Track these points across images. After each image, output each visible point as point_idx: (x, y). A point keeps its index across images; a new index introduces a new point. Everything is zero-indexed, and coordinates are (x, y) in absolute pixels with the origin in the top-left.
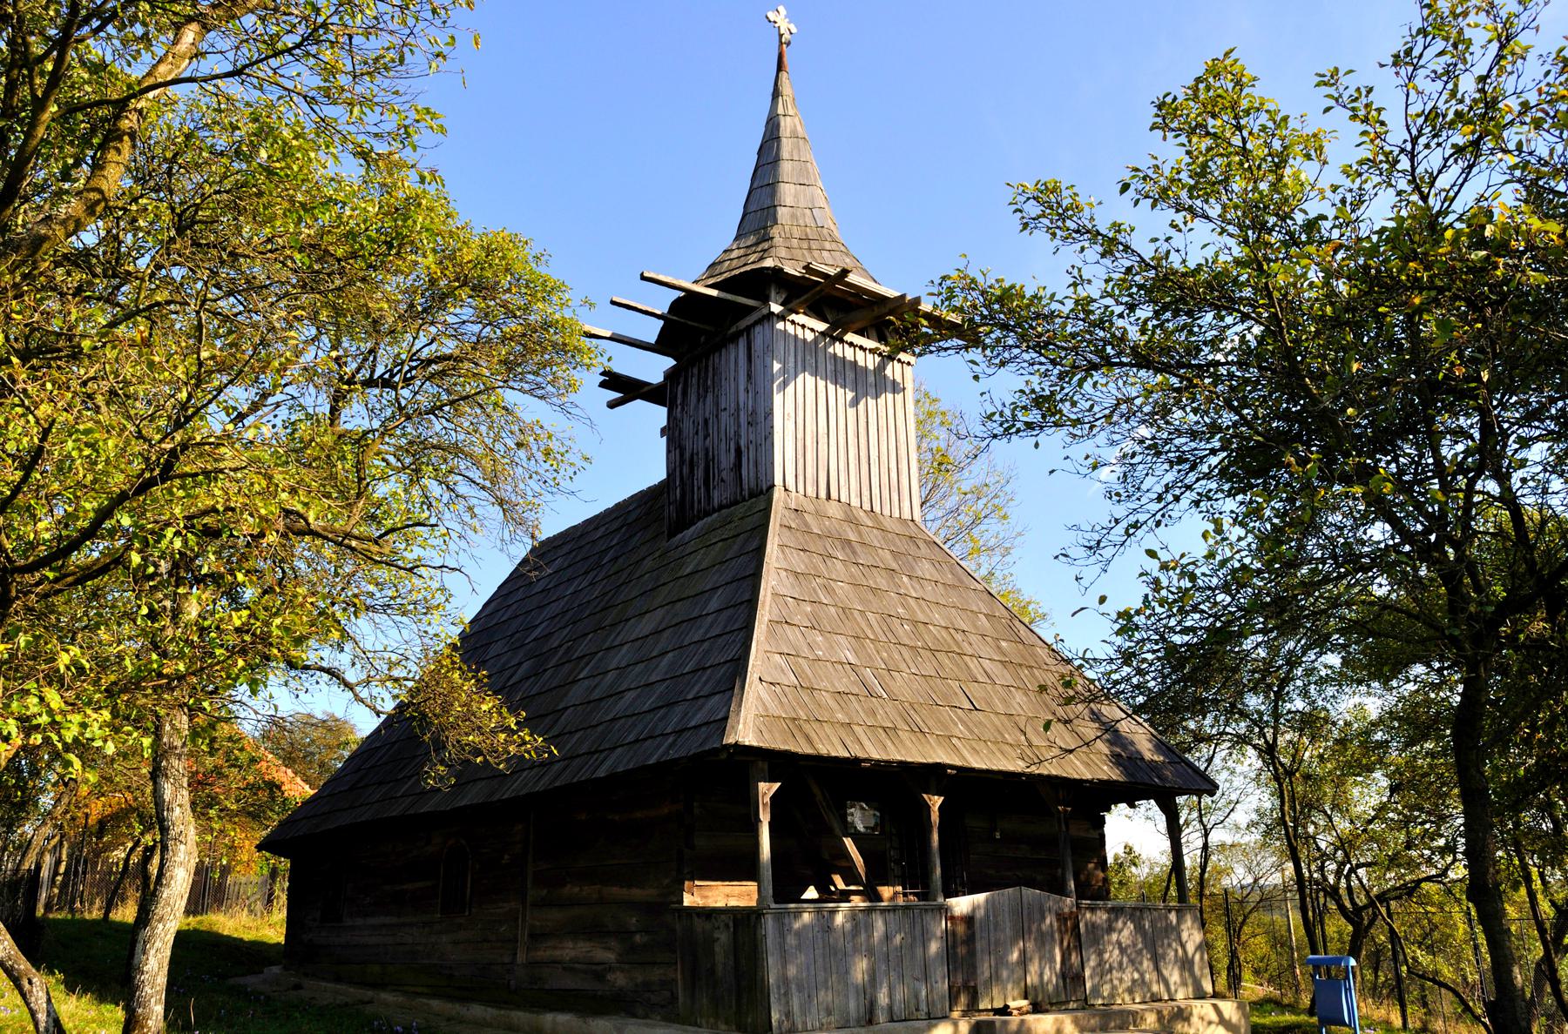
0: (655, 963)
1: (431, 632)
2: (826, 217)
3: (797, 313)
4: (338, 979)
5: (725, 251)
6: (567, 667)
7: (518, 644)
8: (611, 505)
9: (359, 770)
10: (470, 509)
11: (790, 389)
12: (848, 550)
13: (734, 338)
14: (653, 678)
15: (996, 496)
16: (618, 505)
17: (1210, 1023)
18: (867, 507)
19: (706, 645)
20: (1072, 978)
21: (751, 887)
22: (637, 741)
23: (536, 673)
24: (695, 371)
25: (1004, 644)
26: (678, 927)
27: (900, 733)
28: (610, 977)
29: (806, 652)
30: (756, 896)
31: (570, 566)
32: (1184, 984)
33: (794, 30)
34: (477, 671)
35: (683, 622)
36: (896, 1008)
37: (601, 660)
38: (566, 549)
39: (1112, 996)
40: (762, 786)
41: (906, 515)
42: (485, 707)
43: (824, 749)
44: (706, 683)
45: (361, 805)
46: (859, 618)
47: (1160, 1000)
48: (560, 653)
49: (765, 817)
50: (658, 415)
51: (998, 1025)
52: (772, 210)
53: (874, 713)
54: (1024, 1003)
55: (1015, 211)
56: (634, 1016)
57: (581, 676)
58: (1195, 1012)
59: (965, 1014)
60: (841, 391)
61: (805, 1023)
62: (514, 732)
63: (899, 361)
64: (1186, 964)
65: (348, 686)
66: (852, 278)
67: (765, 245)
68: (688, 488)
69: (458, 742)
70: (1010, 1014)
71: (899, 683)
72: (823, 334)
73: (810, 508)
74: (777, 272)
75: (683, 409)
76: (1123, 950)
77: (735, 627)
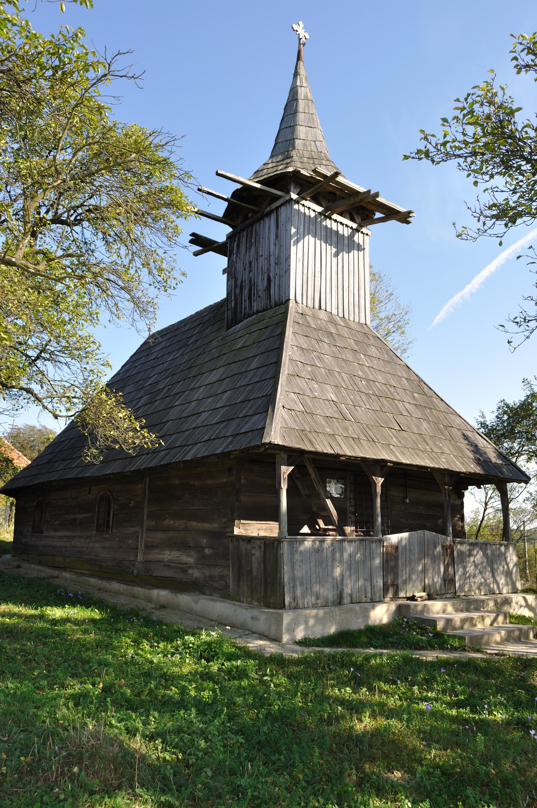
0: (216, 566)
1: (89, 369)
2: (323, 147)
3: (306, 200)
4: (40, 564)
5: (264, 164)
6: (168, 399)
7: (140, 387)
8: (193, 313)
9: (53, 453)
10: (116, 304)
11: (300, 244)
12: (331, 338)
13: (269, 214)
14: (218, 405)
15: (399, 321)
16: (197, 313)
17: (521, 606)
18: (341, 315)
19: (250, 387)
20: (449, 581)
21: (274, 525)
22: (209, 440)
23: (150, 403)
24: (245, 234)
25: (416, 395)
26: (231, 546)
27: (362, 441)
28: (190, 571)
29: (308, 393)
30: (277, 531)
31: (170, 345)
32: (507, 584)
33: (307, 37)
34: (116, 392)
35: (236, 374)
36: (354, 596)
37: (188, 395)
38: (168, 336)
39: (470, 590)
40: (284, 468)
41: (362, 321)
42: (120, 415)
43: (320, 448)
44: (250, 408)
45: (53, 472)
46: (338, 376)
47: (494, 593)
48: (164, 392)
49: (284, 486)
50: (222, 261)
51: (412, 607)
52: (292, 141)
53: (347, 430)
54: (424, 594)
55: (513, 59)
56: (204, 594)
57: (176, 404)
58: (514, 600)
59: (392, 599)
60: (329, 247)
61: (303, 603)
62: (138, 431)
63: (362, 232)
64: (508, 574)
65: (38, 399)
66: (340, 179)
67: (288, 161)
68: (239, 301)
69: (105, 435)
70: (416, 600)
71: (360, 413)
72: (319, 213)
73: (310, 313)
74: (296, 173)
75: (237, 256)
76: (476, 566)
77: (268, 377)
